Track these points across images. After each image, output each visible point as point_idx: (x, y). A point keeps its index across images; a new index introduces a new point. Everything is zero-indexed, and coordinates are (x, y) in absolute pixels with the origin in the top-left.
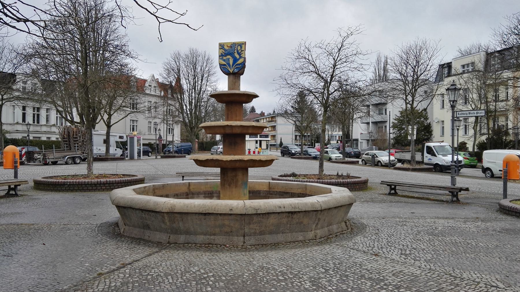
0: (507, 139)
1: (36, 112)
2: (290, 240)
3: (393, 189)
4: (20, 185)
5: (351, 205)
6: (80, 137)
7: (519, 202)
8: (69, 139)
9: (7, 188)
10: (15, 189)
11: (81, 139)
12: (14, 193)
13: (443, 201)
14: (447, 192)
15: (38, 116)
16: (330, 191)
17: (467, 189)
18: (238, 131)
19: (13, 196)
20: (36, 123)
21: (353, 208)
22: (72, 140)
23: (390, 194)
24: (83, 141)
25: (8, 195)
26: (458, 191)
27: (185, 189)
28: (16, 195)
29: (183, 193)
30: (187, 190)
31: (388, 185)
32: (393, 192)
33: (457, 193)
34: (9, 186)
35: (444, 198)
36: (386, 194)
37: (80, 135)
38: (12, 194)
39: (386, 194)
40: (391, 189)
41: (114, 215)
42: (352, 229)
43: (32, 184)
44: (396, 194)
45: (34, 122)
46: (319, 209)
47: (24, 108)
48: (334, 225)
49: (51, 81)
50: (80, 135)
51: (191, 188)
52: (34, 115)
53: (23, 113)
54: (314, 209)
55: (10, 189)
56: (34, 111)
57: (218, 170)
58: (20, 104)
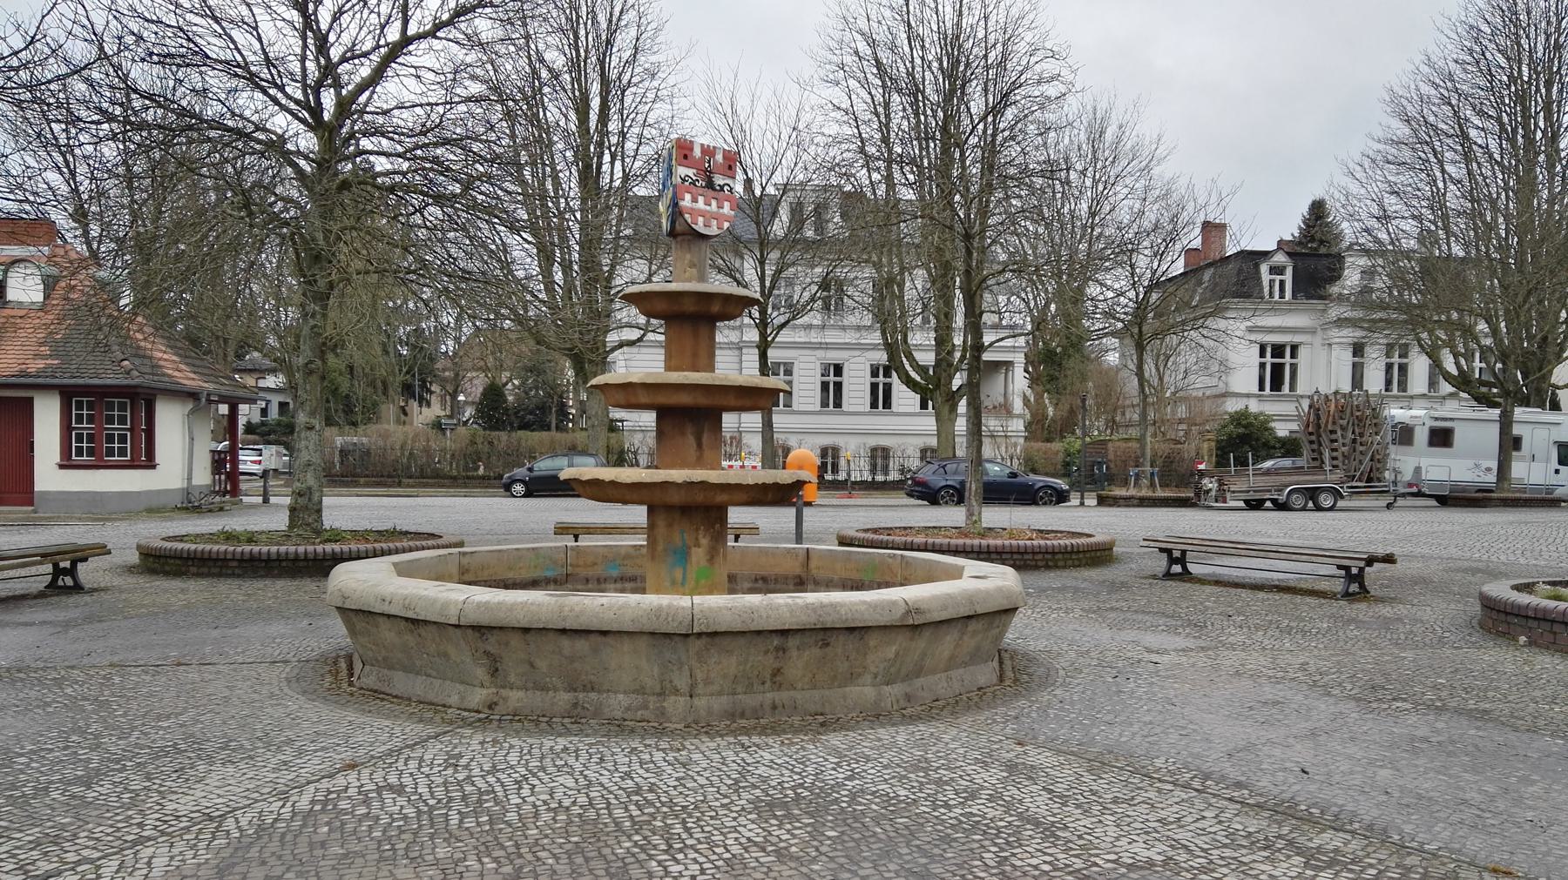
0: (433, 397)
1: (1396, 359)
2: (431, 697)
3: (1176, 563)
4: (85, 560)
5: (1011, 611)
6: (1343, 429)
7: (3, 594)
8: (1319, 436)
9: (49, 568)
10: (72, 572)
11: (1350, 436)
12: (69, 581)
13: (23, 597)
14: (1334, 571)
15: (1403, 369)
16: (956, 573)
17: (1389, 559)
18: (702, 400)
19: (67, 590)
20: (1395, 391)
21: (1017, 620)
22: (1325, 439)
23: (1168, 575)
24: (1354, 441)
25: (54, 588)
26: (1362, 564)
27: (793, 567)
28: (78, 588)
29: (786, 578)
30: (798, 571)
31: (1161, 550)
32: (1177, 569)
33: (1361, 570)
34: (56, 566)
35: (1324, 585)
36: (1154, 577)
37: (1344, 422)
38: (66, 587)
39: (1154, 577)
40: (1172, 561)
41: (337, 633)
42: (1015, 675)
43: (134, 558)
44: (1186, 576)
45: (1261, 388)
46: (454, 621)
47: (1358, 349)
48: (972, 661)
49: (1456, 259)
50: (1344, 422)
51: (813, 564)
52: (1389, 367)
53: (1354, 365)
54: (410, 615)
55: (58, 572)
56: (1388, 355)
57: (637, 514)
58: (1350, 334)
